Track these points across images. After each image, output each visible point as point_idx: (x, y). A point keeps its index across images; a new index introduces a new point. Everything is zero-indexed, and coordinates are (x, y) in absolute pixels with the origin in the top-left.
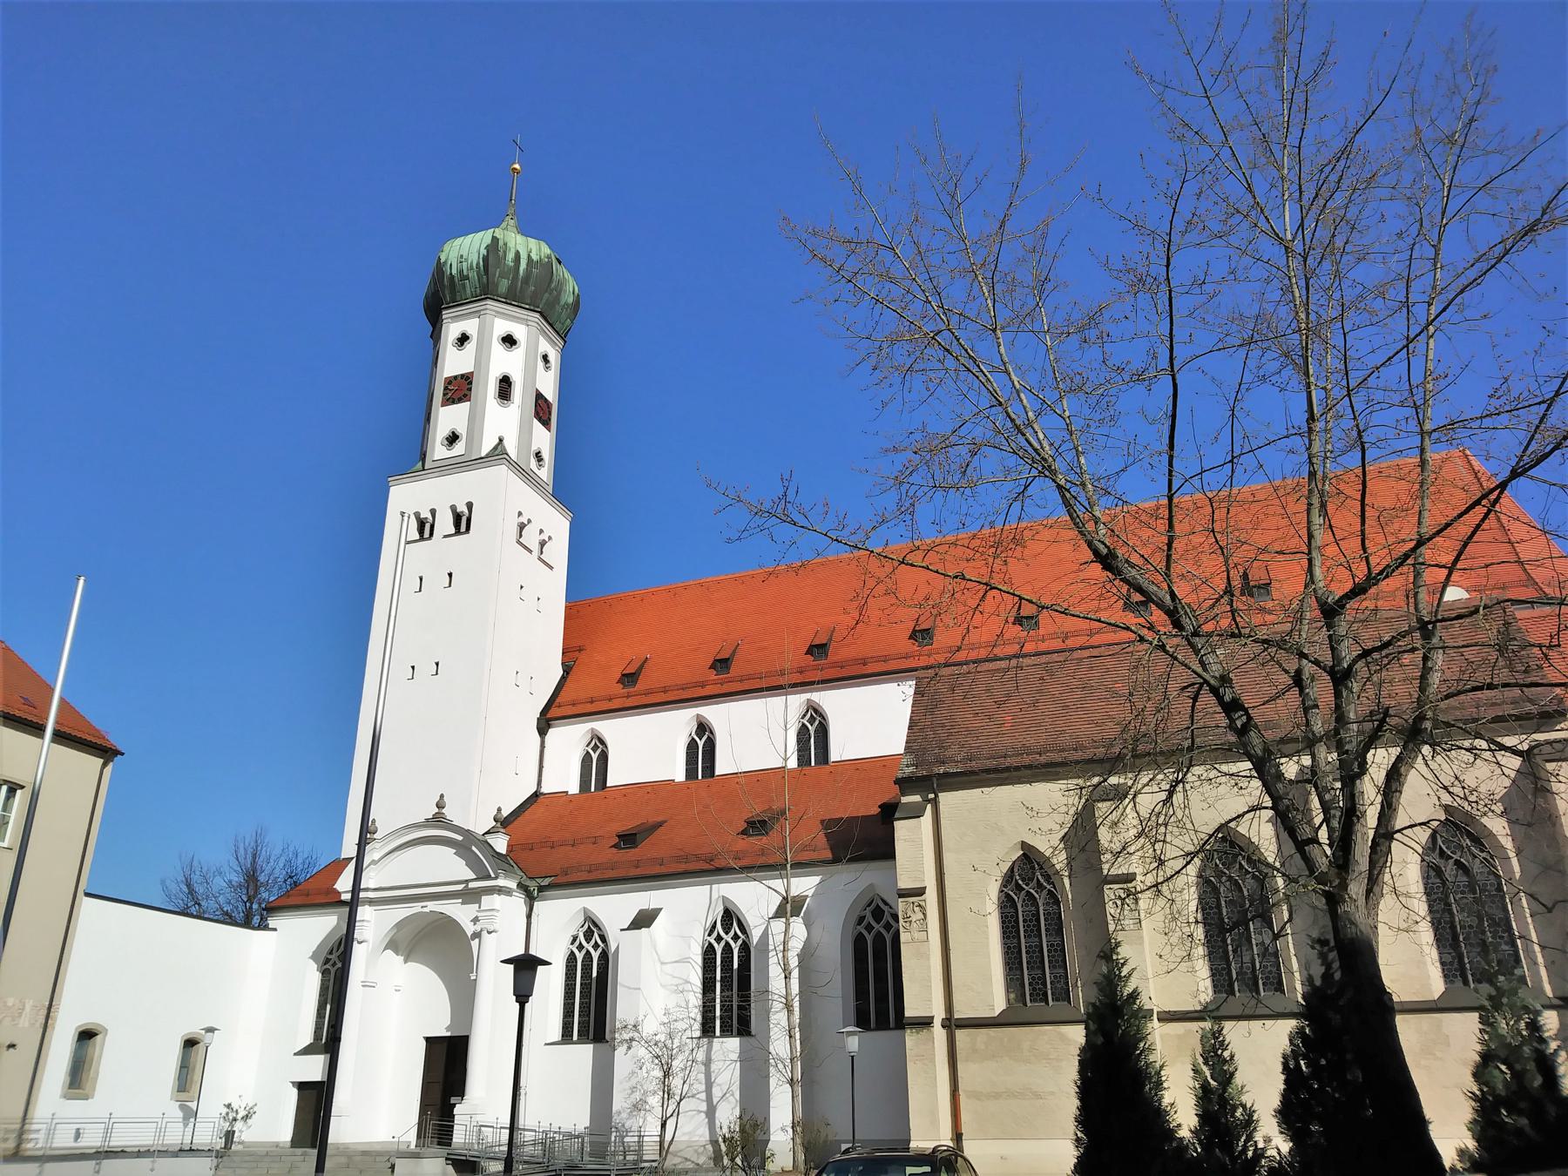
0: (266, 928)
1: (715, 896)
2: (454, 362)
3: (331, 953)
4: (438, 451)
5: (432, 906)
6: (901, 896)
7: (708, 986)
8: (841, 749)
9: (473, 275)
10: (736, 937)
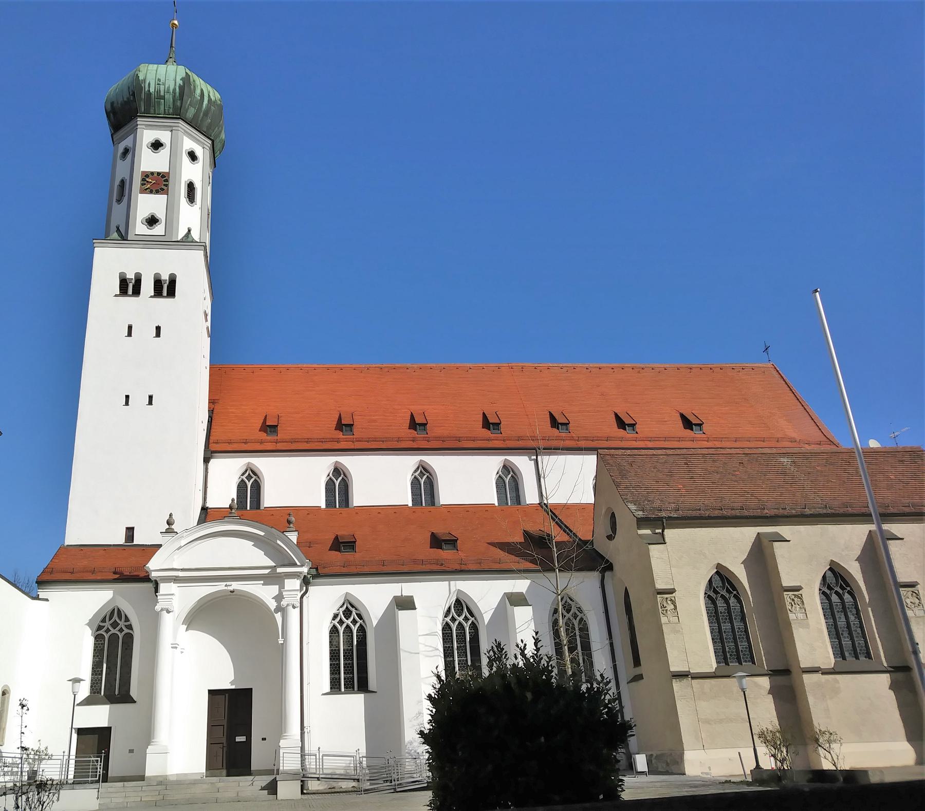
0: (37, 598)
1: (453, 589)
2: (150, 162)
3: (104, 620)
4: (140, 228)
5: (235, 585)
6: (659, 593)
7: (448, 653)
8: (359, 499)
9: (169, 97)
10: (354, 622)
